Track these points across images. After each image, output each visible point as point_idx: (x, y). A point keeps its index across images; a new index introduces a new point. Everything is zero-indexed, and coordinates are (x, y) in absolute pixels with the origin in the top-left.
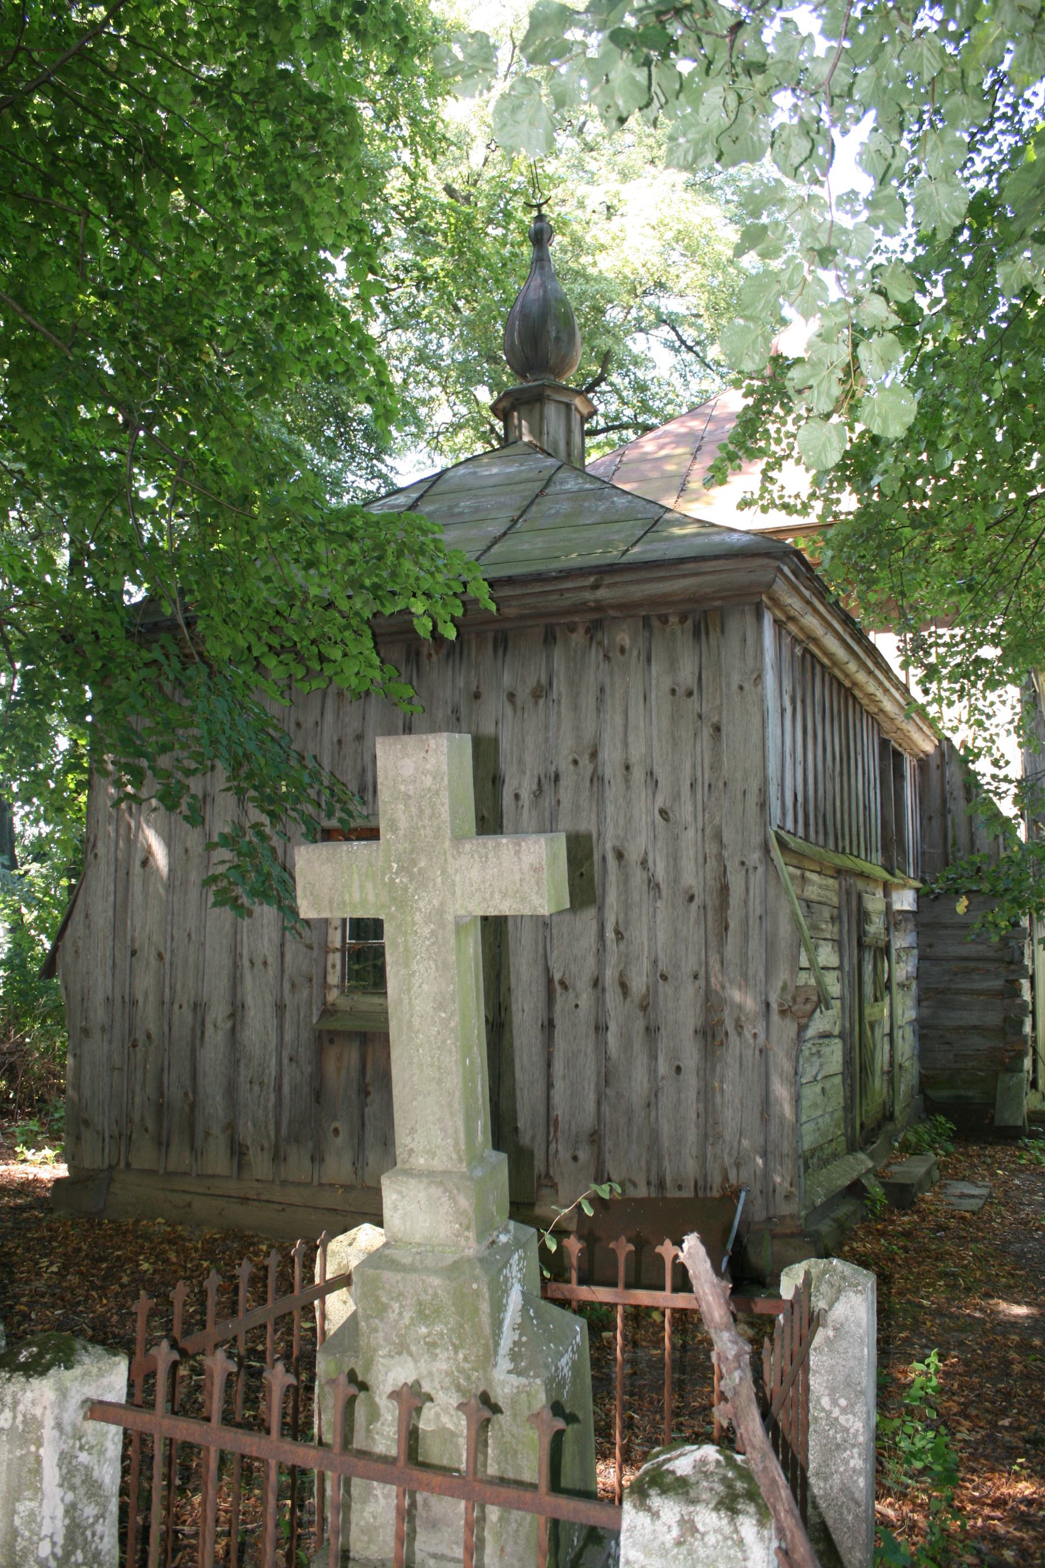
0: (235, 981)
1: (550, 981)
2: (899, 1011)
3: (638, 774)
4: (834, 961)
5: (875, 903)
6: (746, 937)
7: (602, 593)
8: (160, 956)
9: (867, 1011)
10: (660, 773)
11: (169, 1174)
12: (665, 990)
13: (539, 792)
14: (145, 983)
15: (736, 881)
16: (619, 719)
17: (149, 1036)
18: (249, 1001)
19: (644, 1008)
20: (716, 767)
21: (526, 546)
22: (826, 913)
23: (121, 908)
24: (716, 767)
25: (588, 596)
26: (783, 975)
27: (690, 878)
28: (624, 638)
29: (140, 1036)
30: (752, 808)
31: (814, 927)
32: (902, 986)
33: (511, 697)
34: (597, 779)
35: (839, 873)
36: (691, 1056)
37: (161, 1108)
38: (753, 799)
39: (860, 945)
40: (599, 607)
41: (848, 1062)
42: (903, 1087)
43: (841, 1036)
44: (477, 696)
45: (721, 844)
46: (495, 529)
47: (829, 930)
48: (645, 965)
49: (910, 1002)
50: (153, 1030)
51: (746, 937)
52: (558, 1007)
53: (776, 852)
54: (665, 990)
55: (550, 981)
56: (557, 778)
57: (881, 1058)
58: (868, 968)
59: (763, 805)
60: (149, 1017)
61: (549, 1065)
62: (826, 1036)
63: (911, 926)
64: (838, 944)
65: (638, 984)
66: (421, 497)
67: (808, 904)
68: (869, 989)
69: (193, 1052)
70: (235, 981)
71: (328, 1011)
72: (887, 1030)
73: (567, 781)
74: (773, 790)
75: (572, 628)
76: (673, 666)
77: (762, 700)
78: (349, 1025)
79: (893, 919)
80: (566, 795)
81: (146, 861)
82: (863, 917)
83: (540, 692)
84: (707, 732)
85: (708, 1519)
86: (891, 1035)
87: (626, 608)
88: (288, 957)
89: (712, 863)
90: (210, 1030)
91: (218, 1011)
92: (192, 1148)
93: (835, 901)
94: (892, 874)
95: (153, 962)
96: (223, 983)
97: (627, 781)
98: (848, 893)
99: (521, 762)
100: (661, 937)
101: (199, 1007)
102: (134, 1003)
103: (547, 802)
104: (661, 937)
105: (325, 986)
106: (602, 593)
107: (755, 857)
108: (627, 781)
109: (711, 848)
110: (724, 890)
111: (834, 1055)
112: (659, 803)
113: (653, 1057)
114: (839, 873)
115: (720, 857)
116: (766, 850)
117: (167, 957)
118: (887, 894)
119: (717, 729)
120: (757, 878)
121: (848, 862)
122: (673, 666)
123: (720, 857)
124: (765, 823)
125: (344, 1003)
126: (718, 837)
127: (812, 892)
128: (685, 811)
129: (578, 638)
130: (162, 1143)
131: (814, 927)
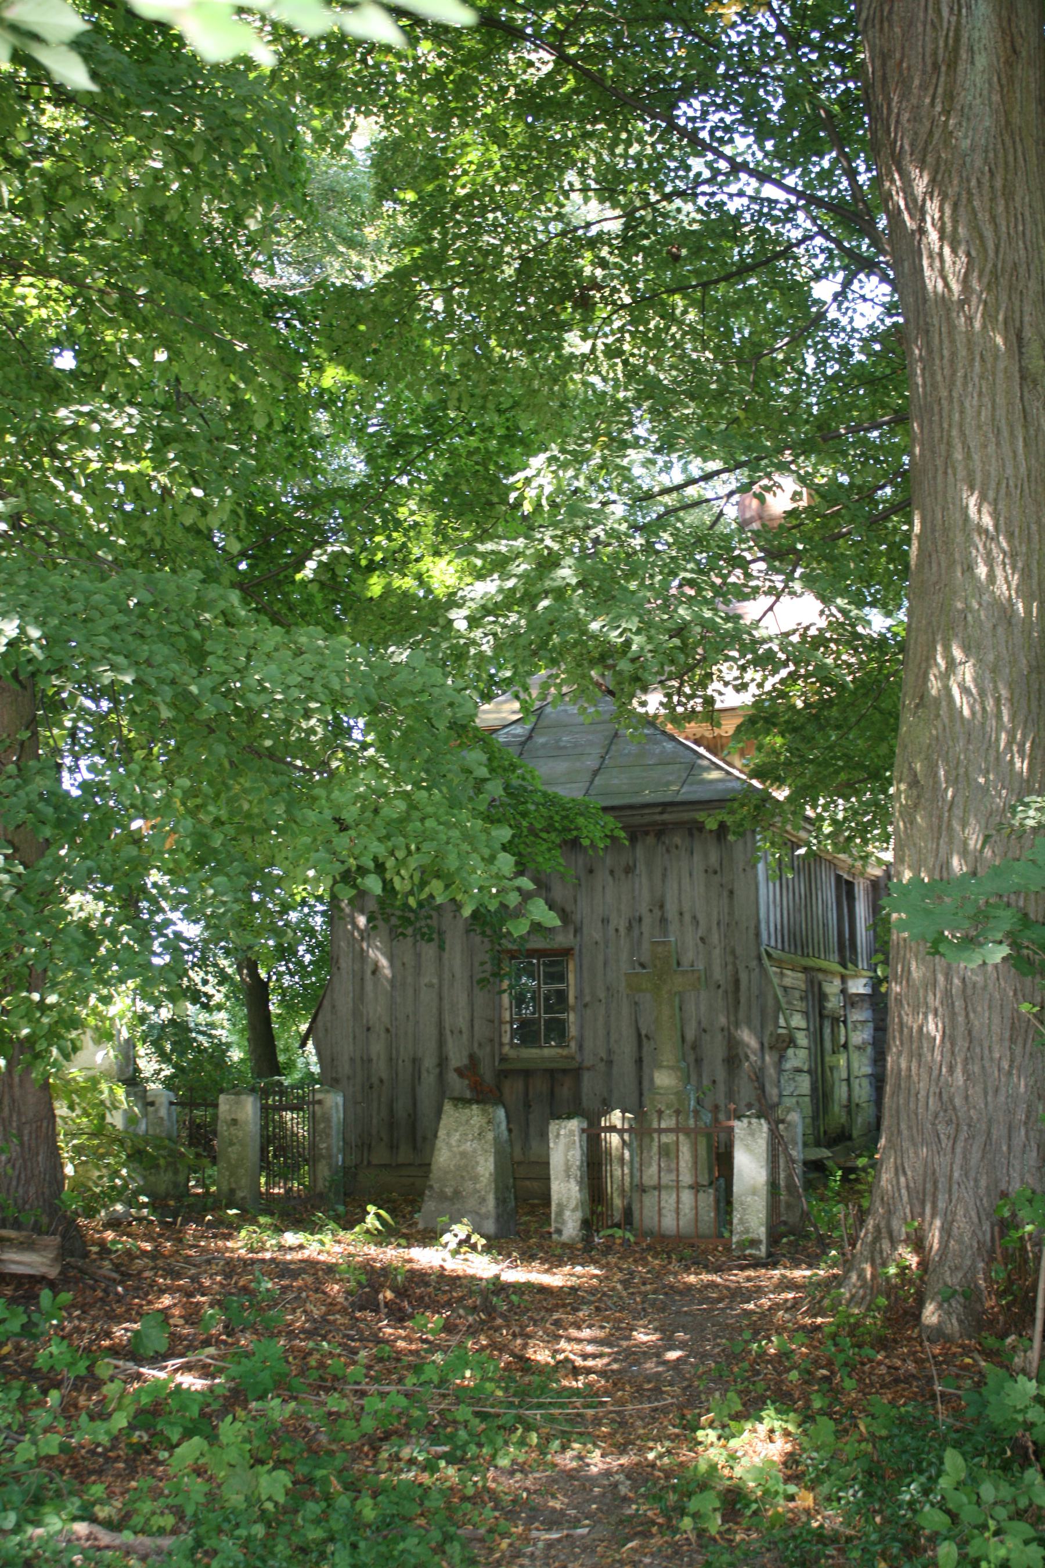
0: (441, 1043)
1: (639, 1035)
2: (855, 1065)
3: (687, 918)
4: (803, 1024)
5: (833, 987)
6: (750, 1007)
7: (666, 817)
8: (388, 1030)
9: (827, 1059)
10: (701, 917)
11: (399, 1166)
12: (706, 1037)
13: (630, 928)
14: (377, 1048)
15: (743, 976)
16: (675, 886)
17: (381, 1081)
18: (451, 1055)
19: (694, 1047)
20: (731, 913)
21: (616, 781)
22: (797, 994)
23: (360, 997)
24: (731, 913)
25: (658, 818)
26: (770, 1028)
27: (718, 974)
28: (677, 840)
29: (375, 1080)
30: (752, 936)
31: (789, 1003)
32: (859, 1048)
33: (612, 872)
34: (663, 920)
35: (806, 970)
36: (721, 1074)
37: (392, 1124)
38: (752, 931)
39: (822, 1016)
40: (664, 823)
41: (814, 1088)
42: (860, 1120)
43: (809, 1072)
44: (591, 871)
45: (735, 957)
46: (592, 763)
47: (799, 1005)
48: (694, 1024)
49: (865, 1061)
50: (384, 1076)
51: (750, 1007)
52: (645, 1049)
53: (766, 961)
54: (706, 1037)
55: (639, 1035)
56: (640, 920)
57: (841, 1092)
58: (827, 1031)
59: (758, 935)
60: (380, 1068)
61: (640, 1083)
62: (799, 1070)
63: (866, 1005)
64: (806, 1014)
65: (690, 1035)
66: (533, 730)
67: (785, 989)
68: (828, 1045)
69: (414, 1089)
70: (441, 1043)
71: (504, 1059)
72: (844, 1075)
73: (647, 920)
74: (763, 926)
75: (647, 833)
76: (706, 855)
77: (756, 876)
78: (519, 1066)
79: (851, 1001)
80: (646, 928)
81: (376, 970)
82: (822, 997)
83: (629, 870)
84: (725, 894)
85: (754, 1121)
86: (848, 1080)
87: (679, 825)
88: (476, 1027)
89: (730, 967)
90: (424, 1075)
91: (429, 1062)
92: (415, 1148)
93: (803, 987)
94: (845, 967)
95: (383, 1035)
96: (432, 1045)
97: (681, 921)
98: (812, 982)
99: (619, 910)
100: (703, 1008)
101: (416, 1061)
102: (370, 1060)
103: (636, 933)
104: (703, 1008)
105: (501, 1044)
106: (666, 817)
107: (754, 964)
108: (681, 921)
109: (730, 959)
110: (737, 982)
111: (804, 1084)
112: (700, 934)
113: (700, 1076)
114: (806, 970)
115: (734, 964)
116: (759, 958)
117: (393, 1030)
118: (844, 979)
119: (731, 892)
120: (755, 975)
121: (810, 962)
122: (706, 855)
123: (734, 964)
124: (758, 943)
125: (512, 1053)
126: (733, 952)
127: (788, 982)
128: (715, 938)
129: (650, 840)
130: (393, 1147)
131: (789, 1003)
